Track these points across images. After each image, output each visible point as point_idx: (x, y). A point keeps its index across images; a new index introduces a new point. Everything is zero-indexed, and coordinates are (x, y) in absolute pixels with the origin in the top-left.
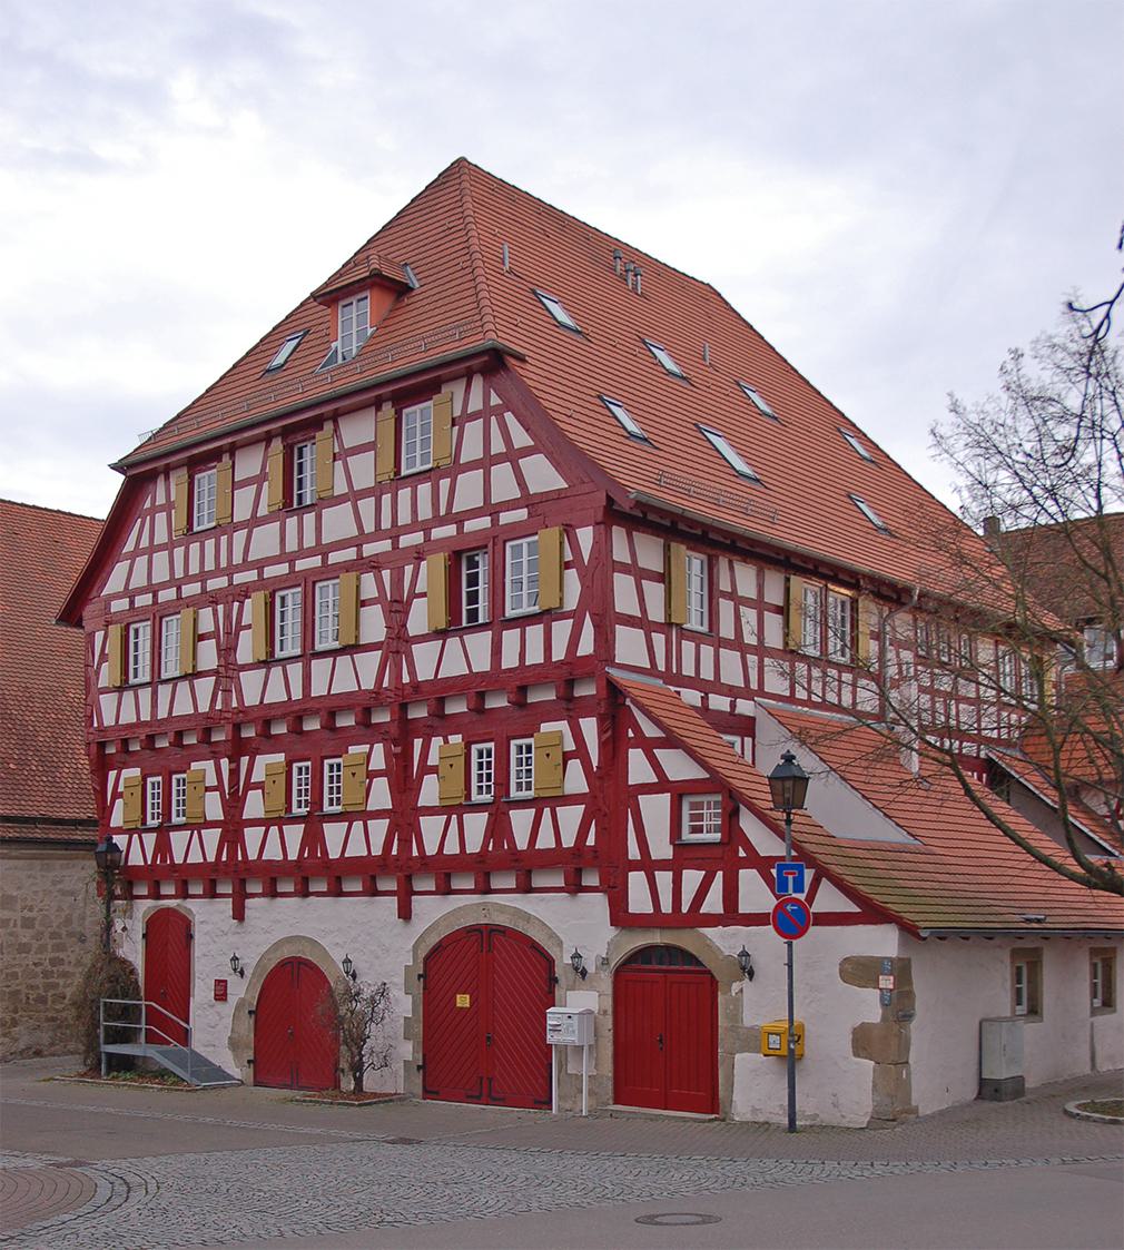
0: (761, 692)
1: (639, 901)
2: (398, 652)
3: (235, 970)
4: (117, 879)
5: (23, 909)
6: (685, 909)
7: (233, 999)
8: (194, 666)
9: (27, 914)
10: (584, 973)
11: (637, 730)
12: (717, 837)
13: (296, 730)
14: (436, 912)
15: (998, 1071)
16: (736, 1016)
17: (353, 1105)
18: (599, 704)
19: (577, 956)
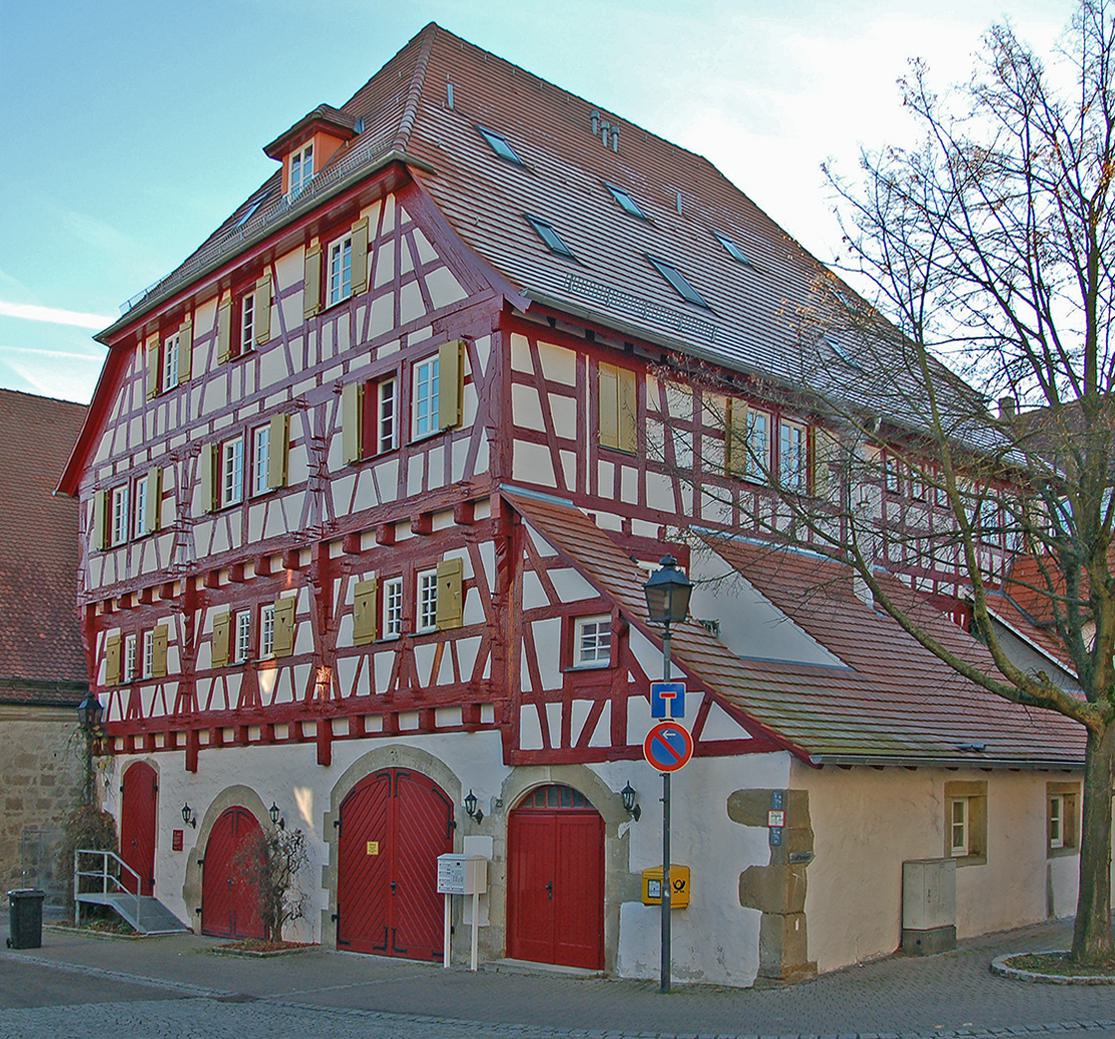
0: (697, 518)
1: (530, 739)
2: (318, 490)
3: (187, 820)
7: (187, 849)
8: (157, 524)
9: (46, 772)
10: (479, 817)
11: (533, 551)
12: (606, 662)
15: (921, 920)
17: (257, 956)
18: (493, 524)
19: (471, 798)
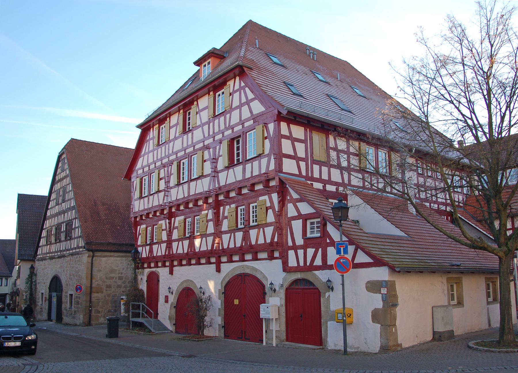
1: (292, 262)
2: (214, 176)
4: (139, 263)
5: (119, 274)
6: (308, 264)
7: (170, 302)
9: (120, 275)
10: (275, 290)
11: (291, 196)
13: (239, 193)
14: (229, 269)
16: (328, 306)
17: (195, 341)
19: (271, 284)
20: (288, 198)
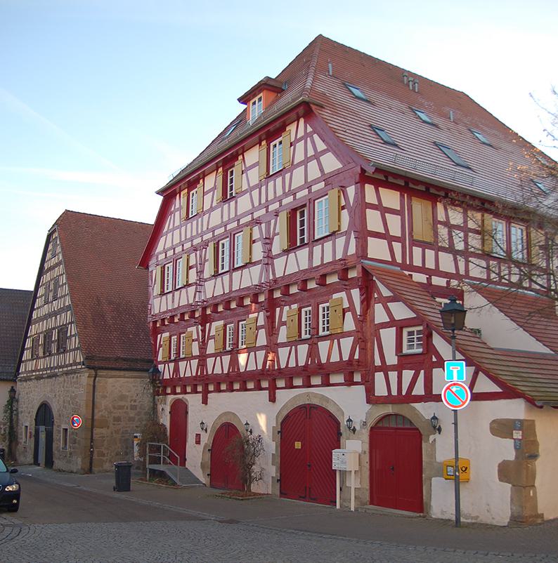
3: (202, 429)
11: (379, 293)
20: (376, 296)
